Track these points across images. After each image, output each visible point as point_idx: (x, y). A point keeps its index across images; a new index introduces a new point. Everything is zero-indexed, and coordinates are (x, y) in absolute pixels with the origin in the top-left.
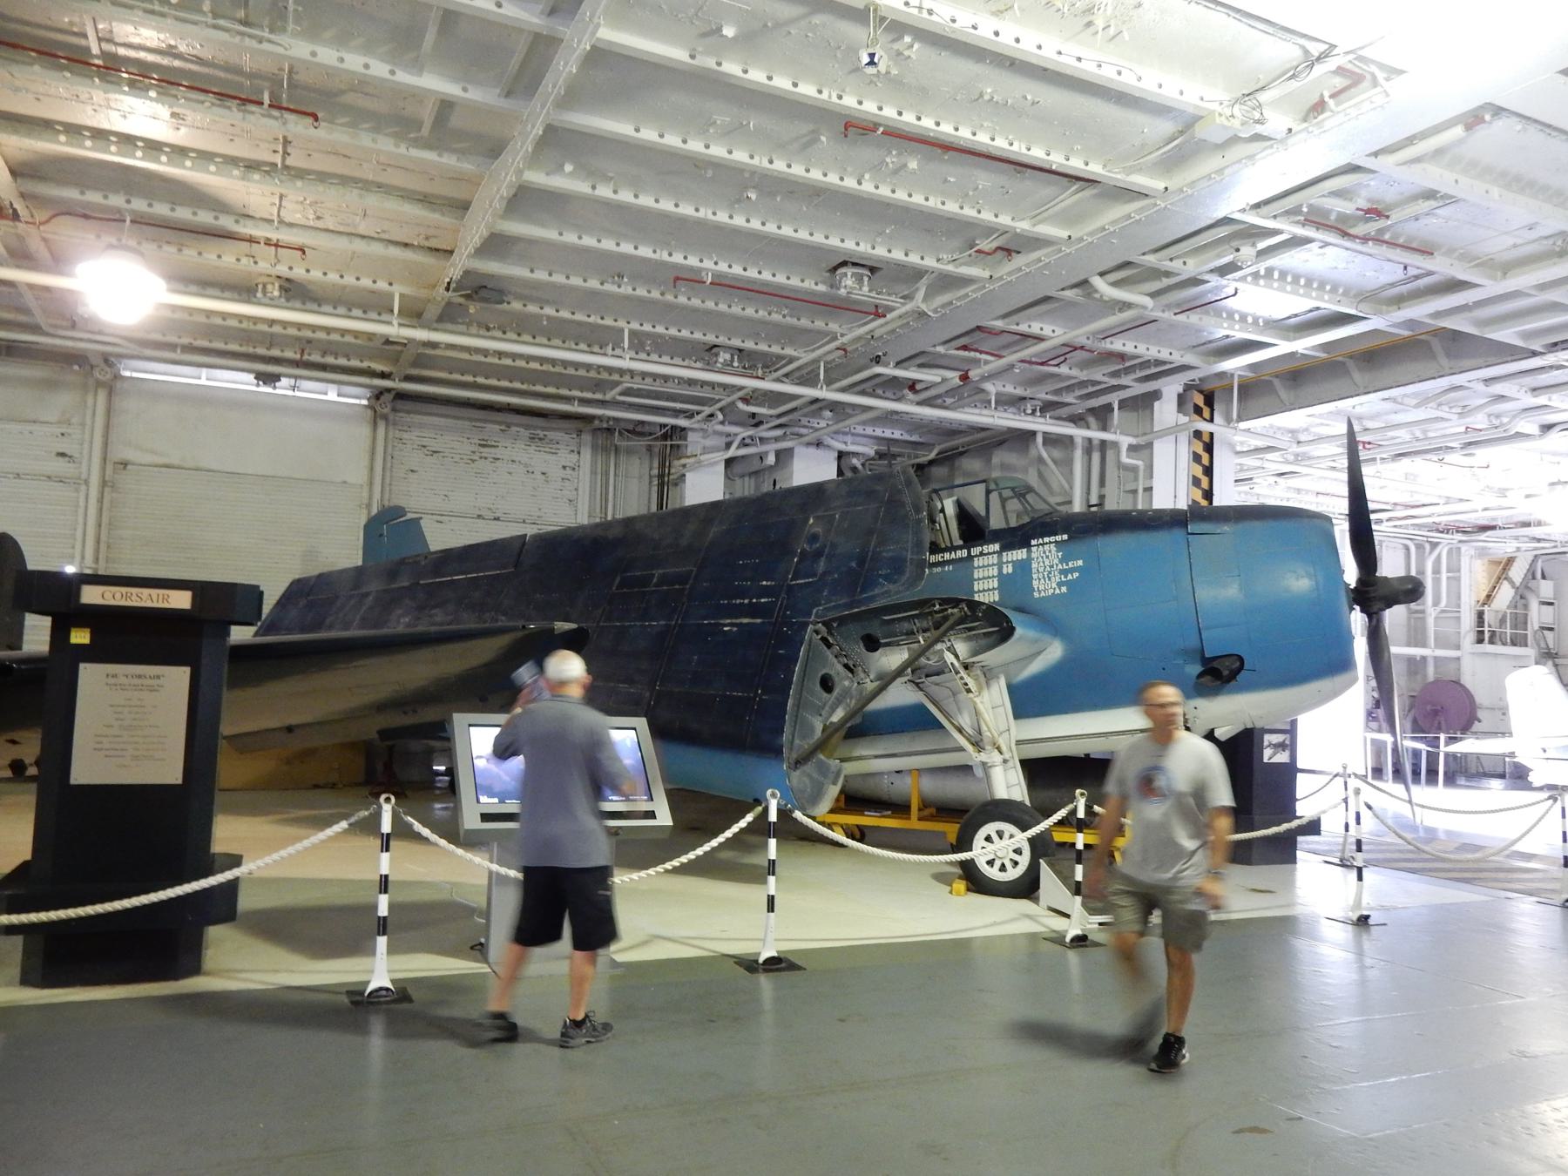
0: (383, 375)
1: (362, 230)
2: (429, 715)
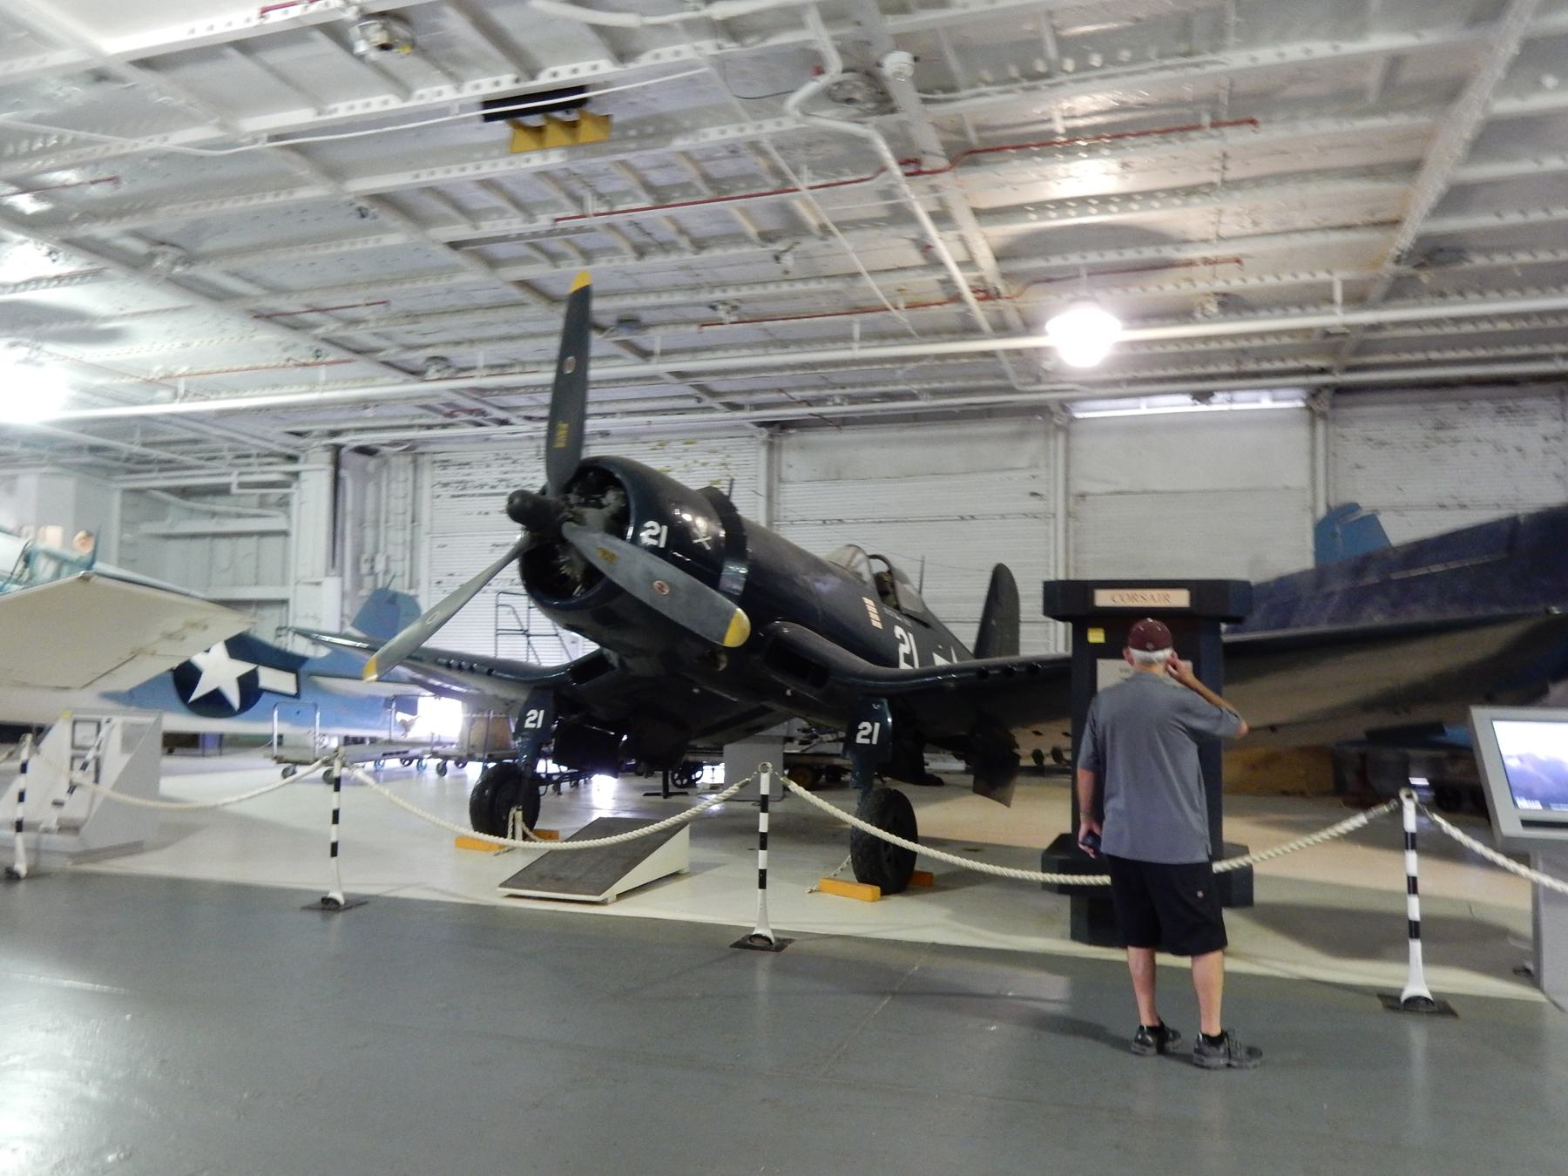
0: (1322, 371)
1: (1300, 224)
2: (1424, 714)
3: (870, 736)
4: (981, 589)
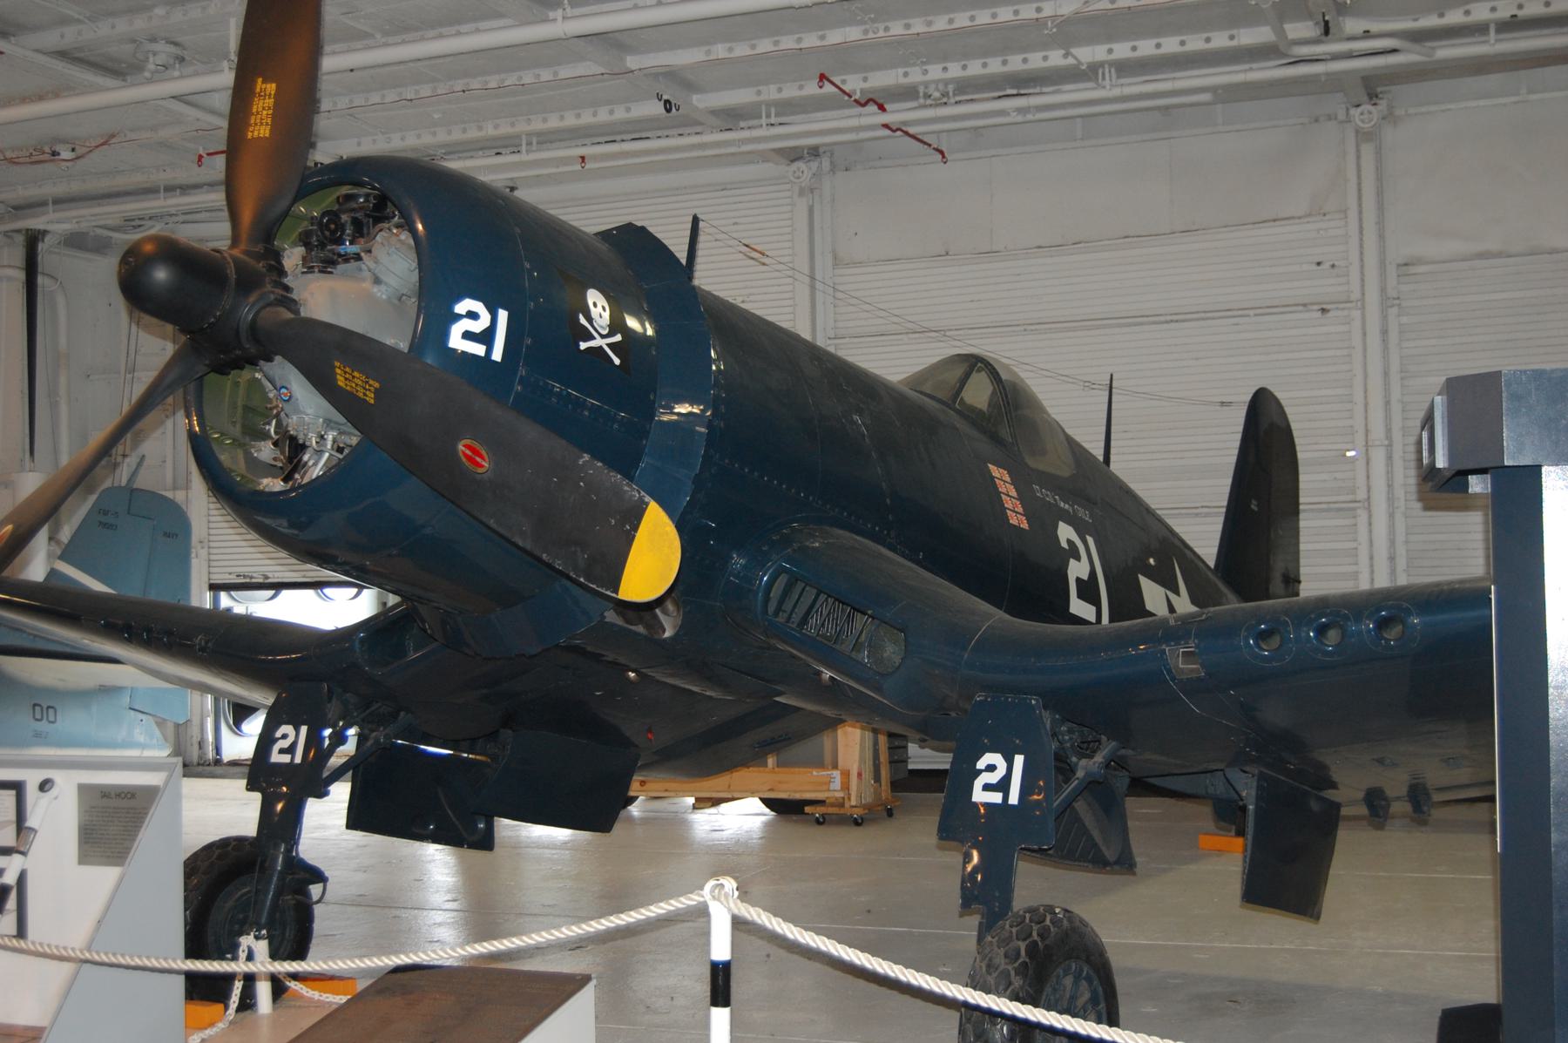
3: (1003, 786)
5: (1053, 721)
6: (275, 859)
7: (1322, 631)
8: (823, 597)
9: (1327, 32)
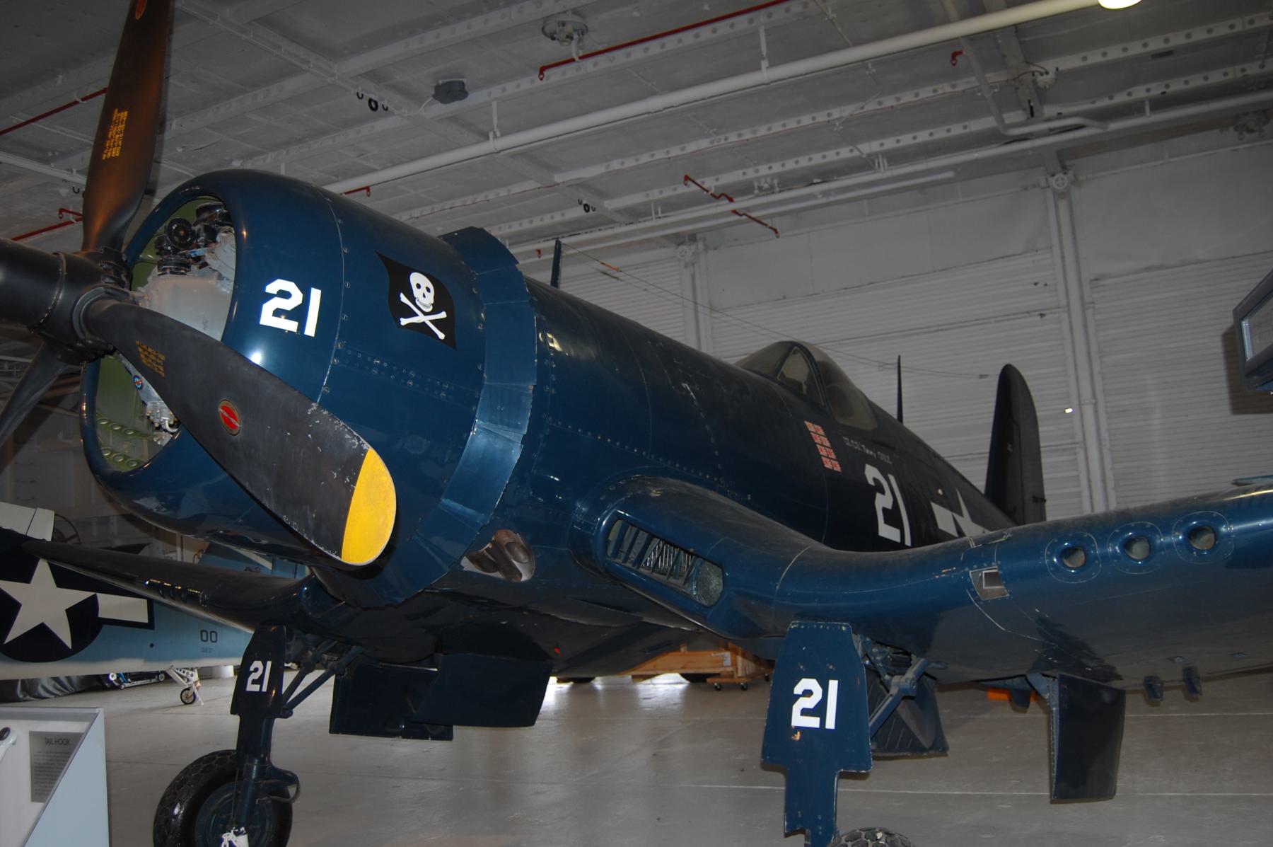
3: (820, 710)
4: (792, 837)
5: (864, 643)
6: (250, 769)
7: (1127, 545)
8: (656, 541)
9: (1032, 115)
